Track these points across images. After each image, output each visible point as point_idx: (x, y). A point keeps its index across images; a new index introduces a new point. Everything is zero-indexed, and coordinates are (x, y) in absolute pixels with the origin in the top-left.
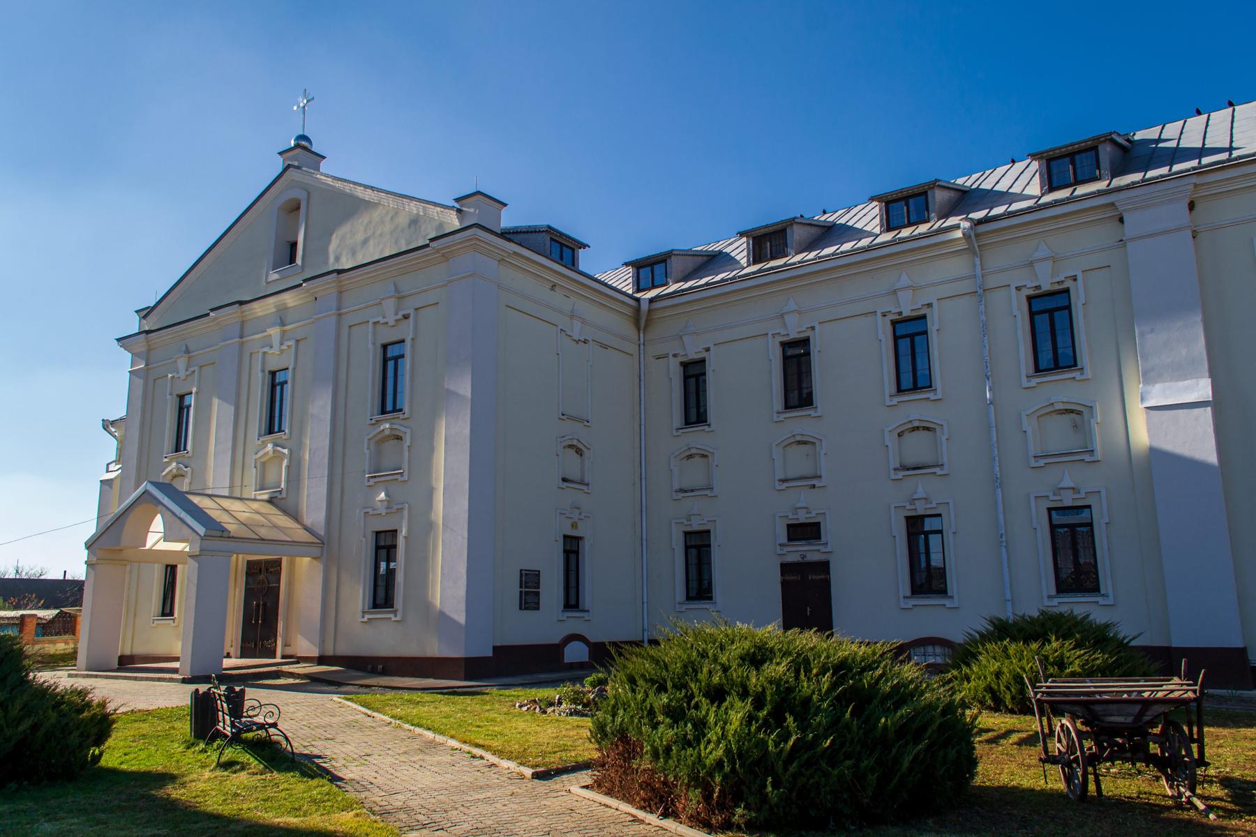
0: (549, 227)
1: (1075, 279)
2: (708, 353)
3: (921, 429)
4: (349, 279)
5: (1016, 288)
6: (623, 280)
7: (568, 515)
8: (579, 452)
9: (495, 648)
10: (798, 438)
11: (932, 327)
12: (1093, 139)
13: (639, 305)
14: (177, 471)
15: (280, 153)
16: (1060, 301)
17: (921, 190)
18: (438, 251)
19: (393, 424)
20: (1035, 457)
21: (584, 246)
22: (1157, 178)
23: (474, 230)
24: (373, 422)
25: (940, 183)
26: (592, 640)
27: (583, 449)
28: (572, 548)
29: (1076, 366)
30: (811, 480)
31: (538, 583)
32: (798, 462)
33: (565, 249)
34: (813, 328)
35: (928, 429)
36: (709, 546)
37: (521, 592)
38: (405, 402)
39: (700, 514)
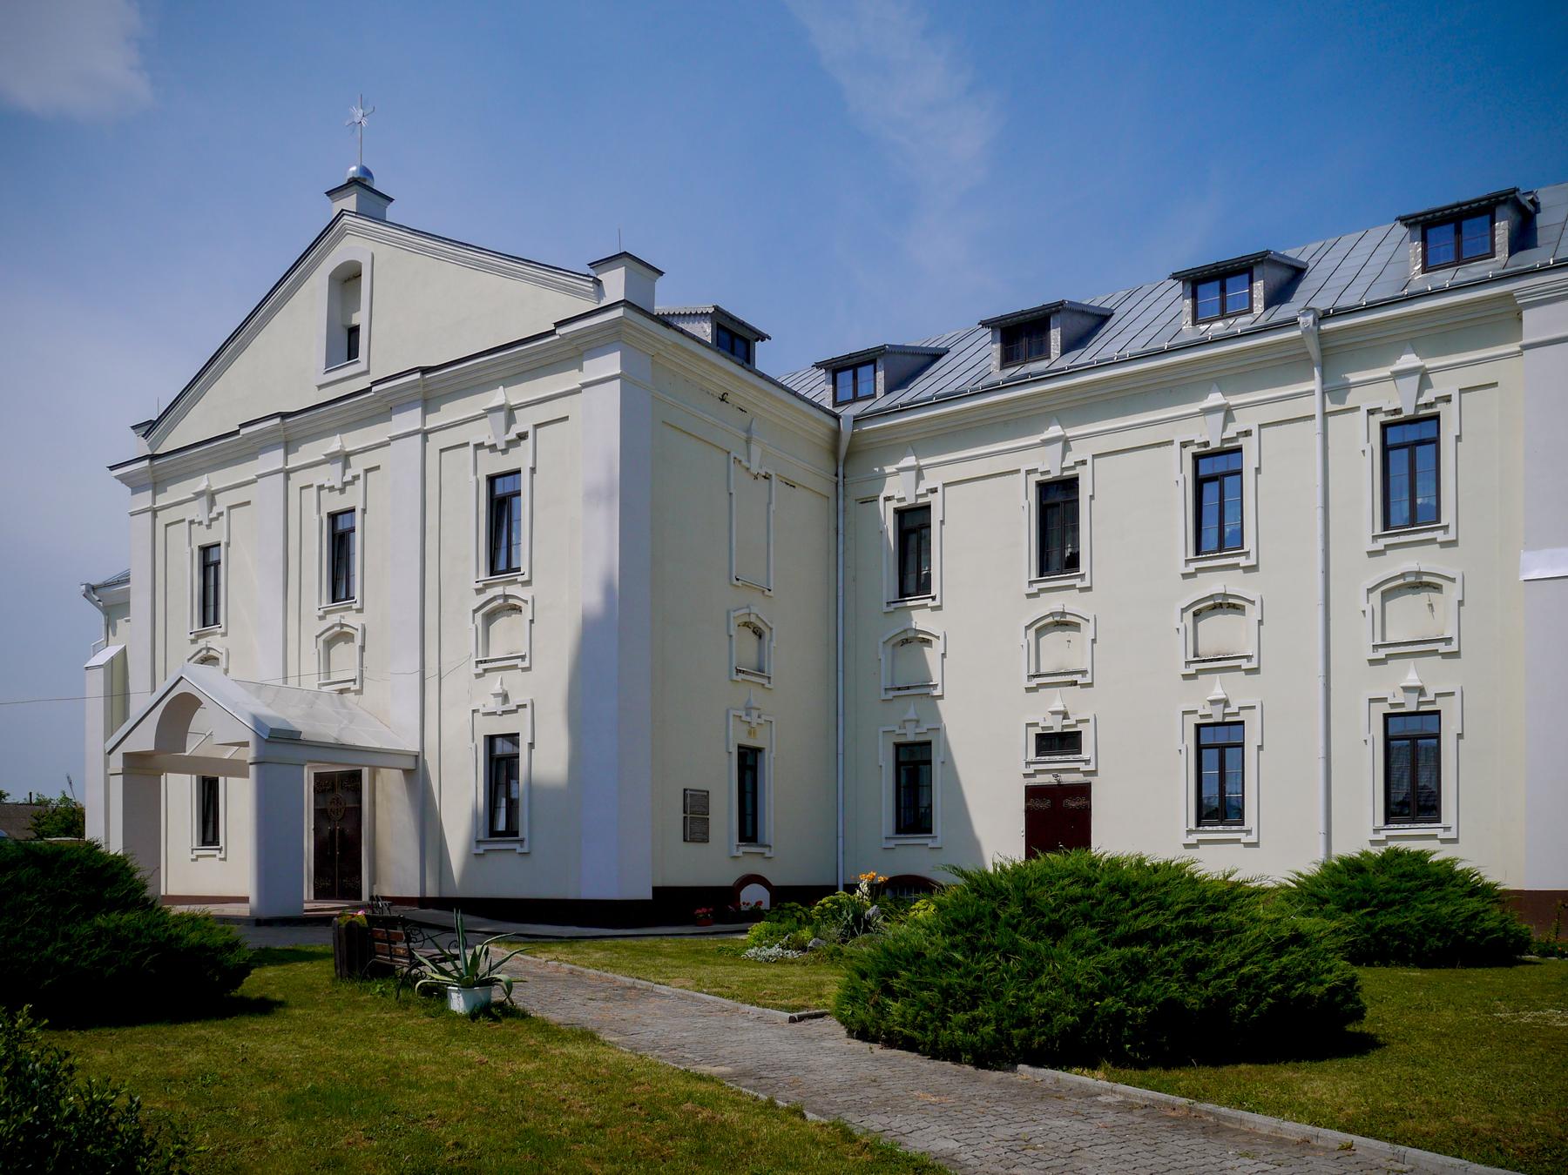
8: (758, 633)
9: (656, 890)
11: (1249, 462)
12: (1488, 198)
16: (1425, 431)
21: (762, 337)
26: (775, 882)
28: (749, 760)
31: (707, 807)
33: (737, 341)
36: (929, 762)
37: (685, 817)
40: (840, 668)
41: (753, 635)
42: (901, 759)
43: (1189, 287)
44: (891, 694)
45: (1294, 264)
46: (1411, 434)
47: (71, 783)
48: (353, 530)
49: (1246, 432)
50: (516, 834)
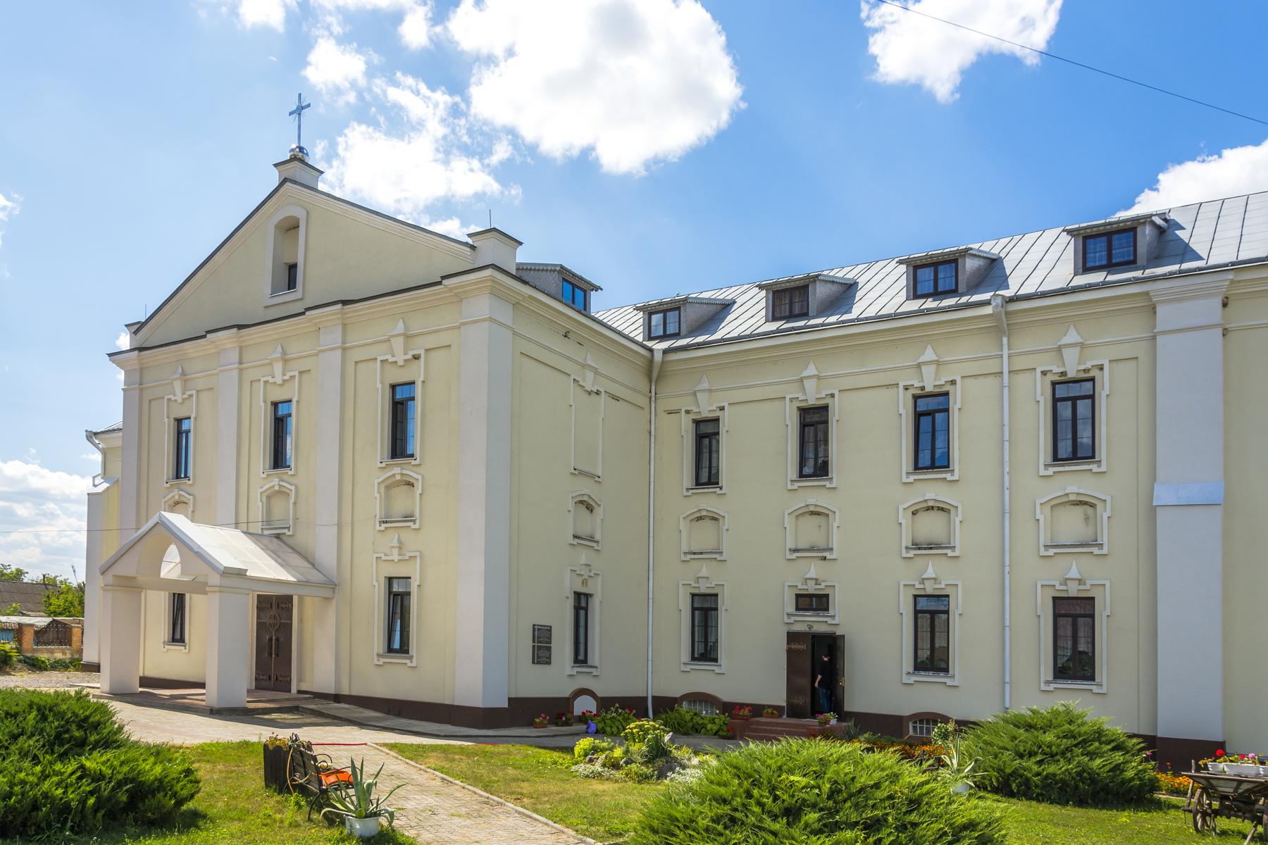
0: (562, 267)
1: (1101, 368)
2: (722, 411)
3: (935, 509)
4: (355, 311)
5: (1042, 372)
6: (631, 324)
7: (578, 572)
10: (812, 509)
13: (653, 355)
14: (179, 498)
15: (276, 165)
17: (952, 257)
18: (451, 290)
19: (403, 469)
20: (1045, 546)
21: (597, 288)
22: (1195, 270)
23: (489, 272)
24: (383, 465)
25: (971, 252)
26: (600, 695)
27: (593, 504)
28: (581, 602)
29: (1094, 458)
30: (821, 552)
31: (550, 638)
32: (810, 532)
33: (576, 289)
34: (832, 396)
35: (942, 509)
36: (716, 609)
37: (534, 646)
38: (415, 445)
39: (708, 576)
40: (651, 535)
41: (586, 510)
42: (696, 606)
43: (911, 269)
44: (689, 557)
45: (989, 256)
46: (1075, 391)
47: (74, 571)
48: (290, 415)
49: (952, 381)
50: (407, 652)
